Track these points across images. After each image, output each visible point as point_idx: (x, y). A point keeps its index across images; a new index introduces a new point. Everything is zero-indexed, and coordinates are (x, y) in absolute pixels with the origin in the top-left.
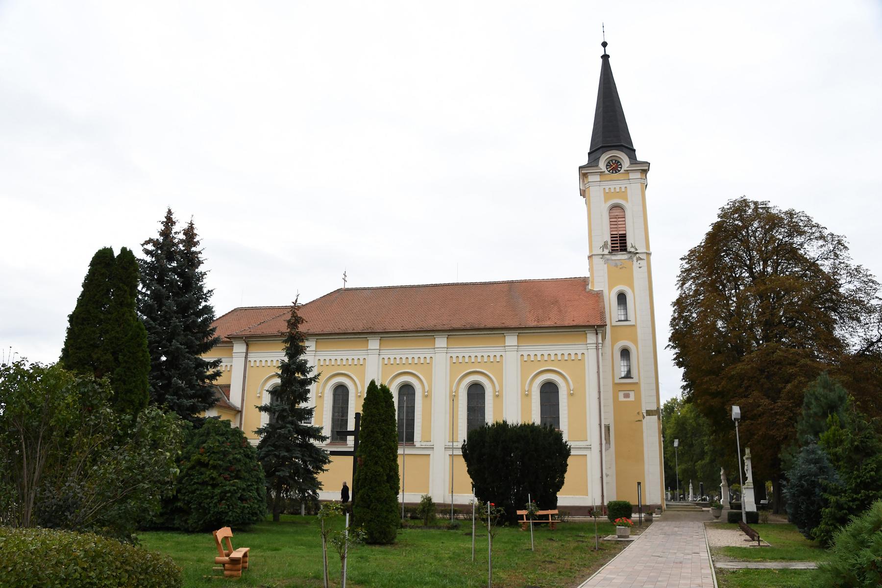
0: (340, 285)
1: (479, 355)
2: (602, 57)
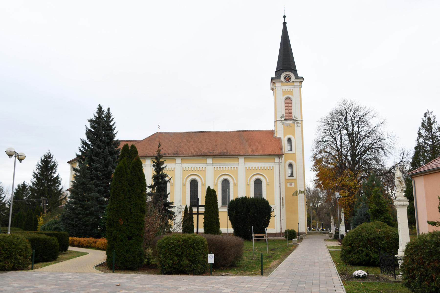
0: (157, 131)
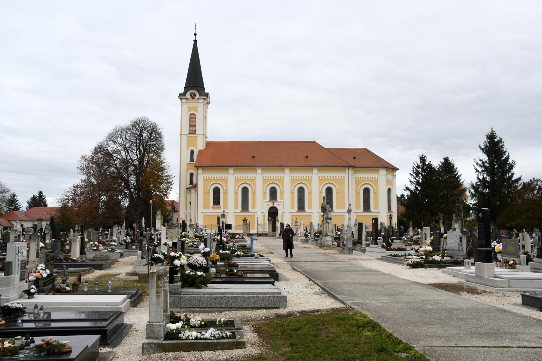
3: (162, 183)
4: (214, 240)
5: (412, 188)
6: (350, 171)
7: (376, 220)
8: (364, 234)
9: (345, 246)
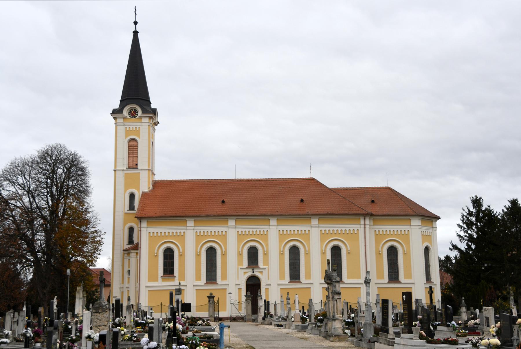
1: (343, 229)
2: (133, 32)
3: (86, 243)
4: (164, 328)
5: (463, 246)
6: (367, 222)
7: (408, 295)
8: (391, 316)
9: (362, 335)
